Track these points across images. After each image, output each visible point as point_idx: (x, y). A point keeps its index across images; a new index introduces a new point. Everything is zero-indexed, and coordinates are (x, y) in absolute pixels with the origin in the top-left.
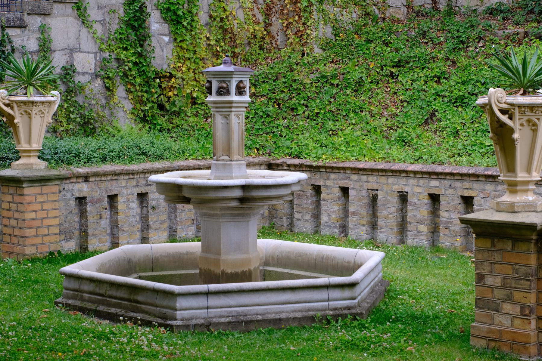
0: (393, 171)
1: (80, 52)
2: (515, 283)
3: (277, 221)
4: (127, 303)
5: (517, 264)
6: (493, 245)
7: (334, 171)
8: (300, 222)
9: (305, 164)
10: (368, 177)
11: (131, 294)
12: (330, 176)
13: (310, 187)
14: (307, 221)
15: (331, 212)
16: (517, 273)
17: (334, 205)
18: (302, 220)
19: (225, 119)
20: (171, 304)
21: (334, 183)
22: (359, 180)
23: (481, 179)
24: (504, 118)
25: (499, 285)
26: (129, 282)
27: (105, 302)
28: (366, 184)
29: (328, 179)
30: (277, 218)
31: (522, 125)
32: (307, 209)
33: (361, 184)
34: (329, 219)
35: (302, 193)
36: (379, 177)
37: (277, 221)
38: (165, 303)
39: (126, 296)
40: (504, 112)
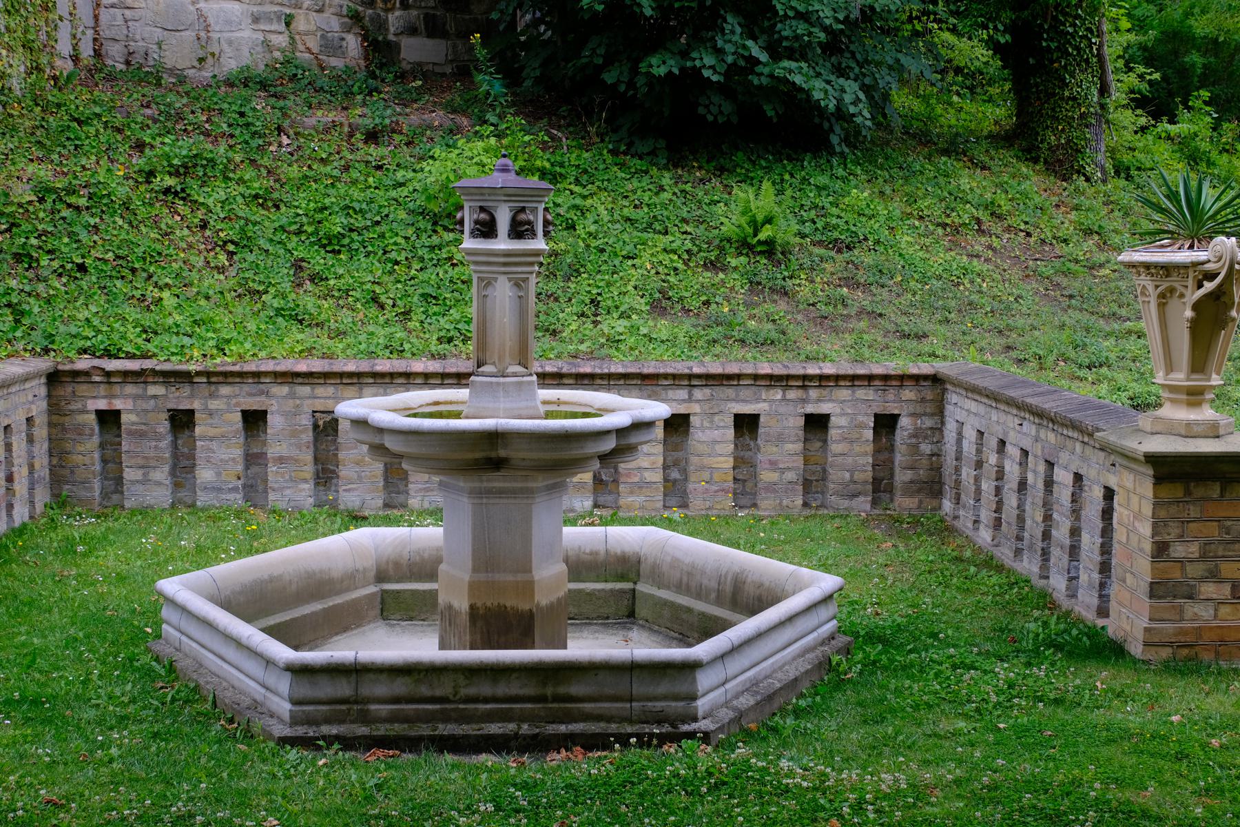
0: (375, 375)
2: (1224, 550)
3: (75, 489)
4: (529, 706)
6: (1188, 492)
7: (230, 380)
8: (140, 488)
9: (158, 368)
10: (313, 389)
11: (545, 684)
12: (217, 390)
13: (166, 415)
14: (159, 484)
15: (221, 460)
16: (1228, 533)
17: (228, 447)
18: (145, 481)
19: (515, 289)
20: (682, 688)
21: (228, 404)
22: (292, 395)
23: (566, 381)
25: (1197, 555)
26: (547, 660)
27: (453, 714)
28: (310, 402)
29: (212, 396)
32: (158, 459)
33: (298, 402)
34: (219, 474)
35: (143, 427)
36: (341, 387)
37: (75, 489)
38: (663, 688)
39: (529, 691)
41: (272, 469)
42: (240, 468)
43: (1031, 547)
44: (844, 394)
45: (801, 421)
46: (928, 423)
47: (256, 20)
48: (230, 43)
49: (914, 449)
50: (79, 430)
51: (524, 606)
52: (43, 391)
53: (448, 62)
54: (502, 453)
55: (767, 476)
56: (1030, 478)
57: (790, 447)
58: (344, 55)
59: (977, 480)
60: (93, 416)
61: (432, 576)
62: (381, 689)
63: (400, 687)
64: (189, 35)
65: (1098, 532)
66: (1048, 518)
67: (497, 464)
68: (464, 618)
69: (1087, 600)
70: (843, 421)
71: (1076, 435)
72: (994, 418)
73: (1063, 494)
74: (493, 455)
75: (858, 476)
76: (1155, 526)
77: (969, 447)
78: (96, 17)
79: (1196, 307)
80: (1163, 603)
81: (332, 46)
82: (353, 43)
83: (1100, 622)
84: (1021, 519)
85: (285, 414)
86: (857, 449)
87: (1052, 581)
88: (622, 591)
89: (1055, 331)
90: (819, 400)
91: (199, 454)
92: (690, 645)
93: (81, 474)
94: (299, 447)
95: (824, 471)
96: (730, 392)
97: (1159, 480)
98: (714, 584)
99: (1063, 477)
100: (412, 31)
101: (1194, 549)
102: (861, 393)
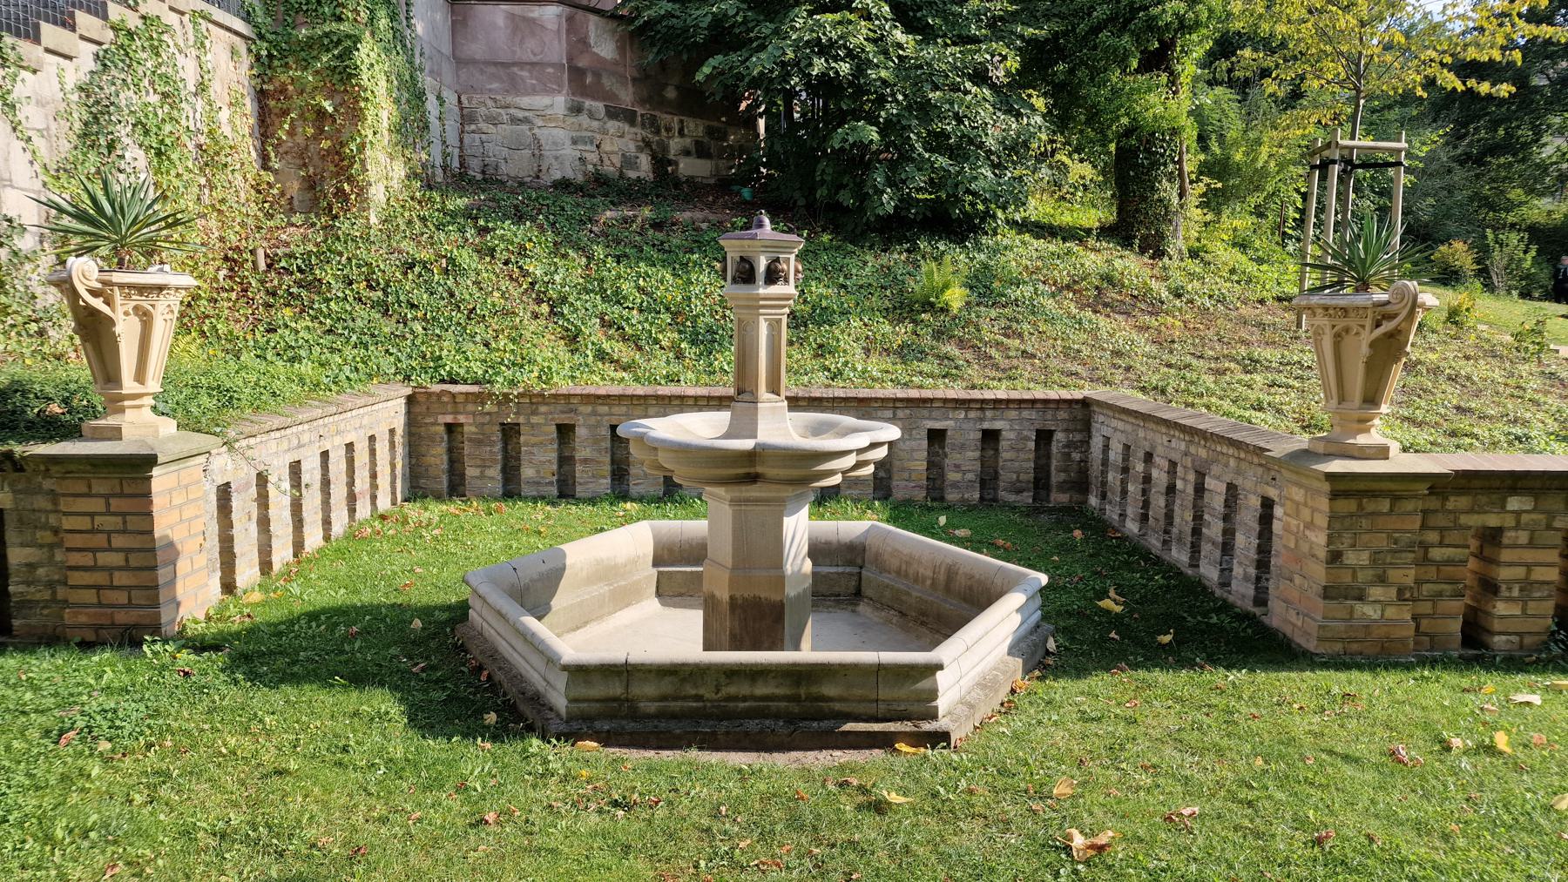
1: (12, 187)
5: (1397, 531)
14: (492, 478)
22: (594, 413)
24: (98, 303)
30: (428, 478)
31: (126, 314)
34: (538, 472)
40: (94, 293)
41: (579, 468)
42: (555, 467)
43: (1180, 540)
44: (1013, 414)
45: (979, 435)
46: (1078, 437)
47: (575, 142)
48: (556, 158)
49: (1067, 456)
50: (432, 438)
51: (775, 597)
52: (403, 409)
53: (712, 176)
54: (759, 469)
55: (952, 476)
56: (1179, 484)
57: (970, 454)
58: (638, 169)
59: (1124, 483)
60: (442, 428)
61: (698, 561)
62: (650, 689)
63: (666, 686)
64: (527, 152)
65: (1255, 534)
66: (1198, 517)
67: (753, 478)
68: (726, 607)
69: (1242, 590)
70: (1012, 435)
71: (1231, 452)
72: (1141, 434)
73: (1216, 501)
74: (752, 470)
75: (1023, 477)
76: (1330, 537)
77: (1115, 455)
78: (461, 141)
79: (1372, 345)
80: (1333, 604)
81: (628, 162)
82: (645, 161)
83: (1257, 611)
84: (1169, 516)
85: (589, 427)
86: (1022, 456)
87: (1202, 570)
88: (851, 574)
89: (4, 448)
90: (993, 419)
91: (523, 457)
92: (930, 650)
93: (432, 472)
94: (599, 451)
95: (996, 472)
96: (925, 413)
97: (1335, 495)
98: (929, 573)
99: (1216, 487)
100: (687, 153)
101: (1364, 558)
102: (1025, 414)
